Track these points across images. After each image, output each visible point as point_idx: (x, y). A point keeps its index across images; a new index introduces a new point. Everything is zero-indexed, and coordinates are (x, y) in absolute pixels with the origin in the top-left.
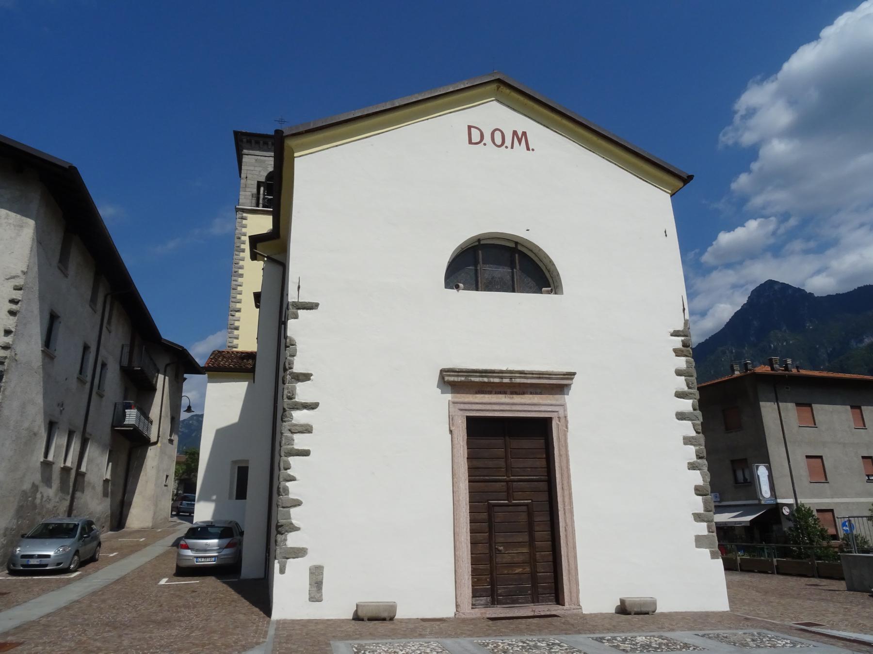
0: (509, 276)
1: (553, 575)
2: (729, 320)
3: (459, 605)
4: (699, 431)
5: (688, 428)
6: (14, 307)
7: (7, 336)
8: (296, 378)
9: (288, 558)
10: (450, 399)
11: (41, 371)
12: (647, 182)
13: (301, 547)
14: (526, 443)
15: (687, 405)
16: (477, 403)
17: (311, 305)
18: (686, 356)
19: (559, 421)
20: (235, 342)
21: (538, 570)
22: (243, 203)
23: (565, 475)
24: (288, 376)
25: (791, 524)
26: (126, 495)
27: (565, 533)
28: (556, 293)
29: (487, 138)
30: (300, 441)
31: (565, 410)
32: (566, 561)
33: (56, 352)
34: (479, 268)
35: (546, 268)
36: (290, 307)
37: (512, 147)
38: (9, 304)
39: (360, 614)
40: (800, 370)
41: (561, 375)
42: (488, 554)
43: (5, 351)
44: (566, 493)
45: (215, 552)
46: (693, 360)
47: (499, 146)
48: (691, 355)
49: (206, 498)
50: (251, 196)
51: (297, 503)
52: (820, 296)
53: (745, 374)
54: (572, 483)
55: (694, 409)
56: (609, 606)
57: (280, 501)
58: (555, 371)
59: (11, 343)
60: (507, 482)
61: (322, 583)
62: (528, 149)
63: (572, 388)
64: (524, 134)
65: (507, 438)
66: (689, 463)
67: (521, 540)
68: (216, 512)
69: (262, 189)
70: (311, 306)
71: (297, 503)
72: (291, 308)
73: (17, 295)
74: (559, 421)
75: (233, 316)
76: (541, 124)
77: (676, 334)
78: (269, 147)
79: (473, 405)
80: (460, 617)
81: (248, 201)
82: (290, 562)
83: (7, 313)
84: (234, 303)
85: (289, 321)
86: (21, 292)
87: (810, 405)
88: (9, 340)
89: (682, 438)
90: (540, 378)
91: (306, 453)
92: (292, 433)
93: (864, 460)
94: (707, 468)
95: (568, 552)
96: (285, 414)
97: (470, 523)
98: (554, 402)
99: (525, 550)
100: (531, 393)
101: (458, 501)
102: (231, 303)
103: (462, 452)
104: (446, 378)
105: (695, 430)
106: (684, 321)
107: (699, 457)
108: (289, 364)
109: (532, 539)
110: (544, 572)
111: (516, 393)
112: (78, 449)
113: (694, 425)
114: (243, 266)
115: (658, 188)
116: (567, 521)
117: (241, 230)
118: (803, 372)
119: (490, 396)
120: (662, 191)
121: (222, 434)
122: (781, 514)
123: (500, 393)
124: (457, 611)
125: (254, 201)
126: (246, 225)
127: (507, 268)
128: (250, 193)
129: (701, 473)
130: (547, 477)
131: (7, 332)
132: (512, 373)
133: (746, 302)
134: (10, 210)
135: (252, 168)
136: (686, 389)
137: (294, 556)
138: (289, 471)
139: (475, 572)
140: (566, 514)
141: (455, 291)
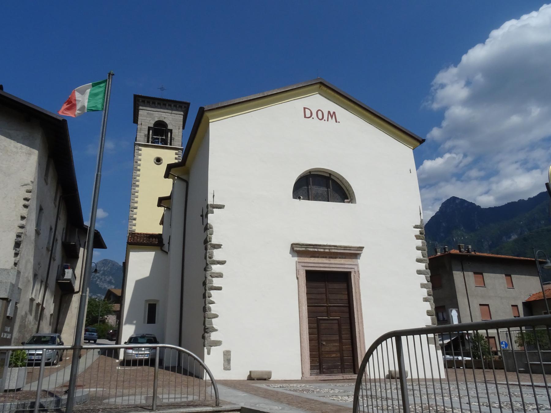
0: (326, 193)
1: (352, 358)
2: (427, 222)
3: (304, 373)
4: (429, 280)
5: (423, 279)
6: (26, 203)
7: (22, 220)
8: (213, 247)
9: (211, 346)
10: (297, 260)
11: (34, 242)
12: (400, 142)
13: (218, 340)
14: (336, 286)
15: (422, 266)
16: (311, 263)
17: (220, 206)
18: (422, 239)
19: (355, 273)
20: (134, 228)
21: (344, 355)
22: (138, 140)
23: (359, 304)
24: (209, 246)
25: (471, 345)
26: (59, 325)
27: (359, 335)
28: (352, 203)
29: (314, 115)
30: (216, 282)
31: (358, 268)
32: (360, 350)
33: (41, 231)
34: (310, 188)
35: (346, 189)
36: (209, 207)
37: (328, 121)
38: (23, 201)
39: (252, 376)
40: (476, 253)
41: (356, 248)
42: (317, 346)
43: (22, 229)
44: (359, 313)
45: (147, 351)
46: (425, 241)
47: (321, 120)
48: (425, 239)
49: (129, 322)
50: (144, 136)
51: (216, 316)
52: (484, 208)
53: (444, 254)
54: (362, 307)
55: (426, 269)
56: (245, 377)
57: (206, 314)
58: (352, 246)
59: (25, 224)
60: (327, 307)
61: (230, 360)
62: (336, 122)
63: (361, 256)
64: (334, 113)
65: (326, 282)
66: (423, 298)
67: (334, 339)
68: (136, 331)
69: (151, 132)
70: (221, 207)
71: (216, 316)
72: (209, 207)
73: (28, 195)
74: (355, 273)
75: (132, 211)
76: (343, 108)
77: (416, 227)
78: (151, 105)
79: (309, 264)
80: (304, 379)
81: (142, 139)
82: (213, 348)
83: (23, 206)
84: (133, 203)
85: (208, 215)
86: (30, 194)
87: (482, 274)
88: (23, 222)
89: (420, 284)
90: (344, 250)
91: (219, 289)
92: (212, 277)
93: (513, 307)
94: (433, 301)
95: (360, 345)
96: (208, 267)
97: (309, 329)
98: (352, 263)
99: (337, 344)
100: (340, 258)
101: (302, 316)
102: (131, 203)
103: (303, 289)
104: (295, 249)
105: (427, 280)
106: (420, 220)
107: (429, 295)
108: (209, 239)
109: (340, 337)
110: (348, 357)
111: (332, 258)
112: (44, 290)
113: (426, 278)
114: (139, 180)
115: (406, 145)
116: (360, 328)
117: (138, 157)
118: (478, 254)
119: (318, 259)
120: (408, 147)
121: (139, 283)
122: (465, 339)
123: (323, 257)
124: (302, 376)
125: (146, 139)
126: (141, 154)
127: (325, 188)
128: (143, 134)
129: (430, 304)
130: (348, 305)
131: (23, 218)
132: (330, 246)
133: (438, 211)
134: (23, 144)
135: (145, 118)
136: (422, 257)
137: (215, 345)
138: (211, 299)
139: (311, 356)
140: (359, 324)
141: (298, 200)
